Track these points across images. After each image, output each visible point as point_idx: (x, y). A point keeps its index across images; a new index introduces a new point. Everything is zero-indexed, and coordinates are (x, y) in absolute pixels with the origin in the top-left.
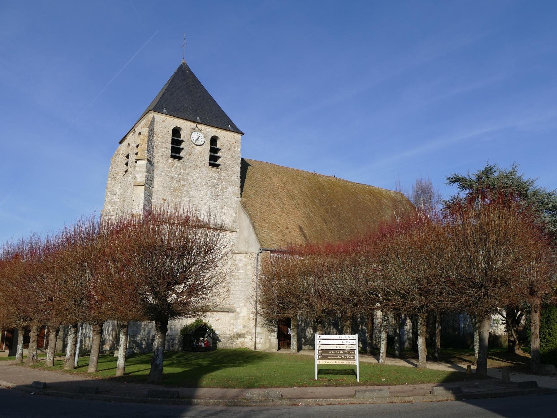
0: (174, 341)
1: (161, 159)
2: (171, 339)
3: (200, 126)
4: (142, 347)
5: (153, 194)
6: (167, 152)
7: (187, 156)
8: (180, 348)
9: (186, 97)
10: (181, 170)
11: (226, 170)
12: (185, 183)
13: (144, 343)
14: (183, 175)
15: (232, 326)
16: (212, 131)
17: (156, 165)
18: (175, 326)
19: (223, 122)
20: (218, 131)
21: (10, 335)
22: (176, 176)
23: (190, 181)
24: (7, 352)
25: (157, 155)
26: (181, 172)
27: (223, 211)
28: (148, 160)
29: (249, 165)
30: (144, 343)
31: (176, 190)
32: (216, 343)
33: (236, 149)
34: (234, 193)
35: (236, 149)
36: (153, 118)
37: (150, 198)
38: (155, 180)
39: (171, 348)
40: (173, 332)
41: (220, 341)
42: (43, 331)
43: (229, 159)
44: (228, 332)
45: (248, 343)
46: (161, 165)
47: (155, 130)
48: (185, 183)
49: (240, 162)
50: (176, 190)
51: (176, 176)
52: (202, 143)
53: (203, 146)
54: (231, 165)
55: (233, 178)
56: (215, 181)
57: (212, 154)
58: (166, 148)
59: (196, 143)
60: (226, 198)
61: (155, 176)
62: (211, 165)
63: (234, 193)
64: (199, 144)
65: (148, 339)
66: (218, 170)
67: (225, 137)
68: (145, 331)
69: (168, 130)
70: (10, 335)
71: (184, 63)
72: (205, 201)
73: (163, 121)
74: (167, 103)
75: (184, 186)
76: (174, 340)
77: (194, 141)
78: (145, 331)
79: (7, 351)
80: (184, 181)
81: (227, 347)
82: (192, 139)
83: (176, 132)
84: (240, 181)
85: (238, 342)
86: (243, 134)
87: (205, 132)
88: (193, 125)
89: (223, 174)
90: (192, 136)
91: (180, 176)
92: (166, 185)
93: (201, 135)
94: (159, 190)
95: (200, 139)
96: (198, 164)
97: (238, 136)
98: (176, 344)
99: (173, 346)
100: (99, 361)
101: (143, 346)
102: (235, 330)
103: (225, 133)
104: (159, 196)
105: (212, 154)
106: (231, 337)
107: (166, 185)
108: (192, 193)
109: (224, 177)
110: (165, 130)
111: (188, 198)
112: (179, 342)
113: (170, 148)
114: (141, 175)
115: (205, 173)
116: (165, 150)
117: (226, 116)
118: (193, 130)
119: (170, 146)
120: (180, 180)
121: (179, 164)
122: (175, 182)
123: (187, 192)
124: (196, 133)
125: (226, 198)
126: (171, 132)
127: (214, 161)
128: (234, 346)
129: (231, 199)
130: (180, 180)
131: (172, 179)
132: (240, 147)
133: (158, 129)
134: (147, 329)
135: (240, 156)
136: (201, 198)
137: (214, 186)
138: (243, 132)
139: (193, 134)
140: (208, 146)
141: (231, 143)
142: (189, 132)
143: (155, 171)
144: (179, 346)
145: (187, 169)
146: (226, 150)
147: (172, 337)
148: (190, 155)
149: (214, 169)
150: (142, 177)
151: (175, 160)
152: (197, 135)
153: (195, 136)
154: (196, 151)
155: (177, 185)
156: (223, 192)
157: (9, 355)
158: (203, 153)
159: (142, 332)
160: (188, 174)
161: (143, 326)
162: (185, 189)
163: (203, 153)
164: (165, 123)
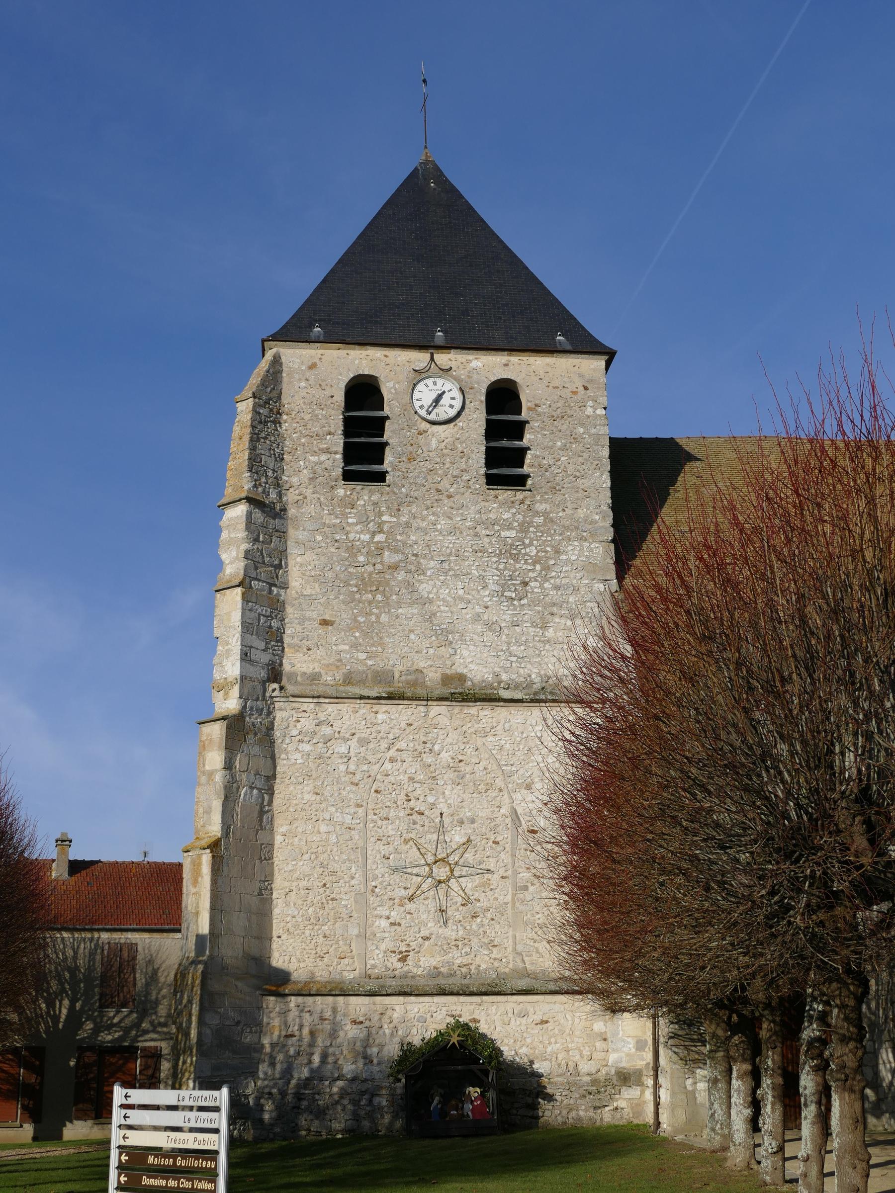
0: (376, 1100)
1: (308, 492)
2: (363, 1093)
3: (442, 358)
4: (261, 1120)
5: (289, 610)
6: (328, 464)
7: (403, 466)
8: (398, 1124)
9: (431, 270)
10: (380, 514)
11: (554, 490)
12: (400, 557)
13: (269, 1106)
14: (390, 532)
15: (599, 1044)
16: (488, 367)
17: (292, 512)
18: (381, 1046)
19: (547, 326)
20: (515, 359)
21: (33, 1079)
22: (366, 537)
23: (417, 549)
24: (28, 1129)
25: (295, 480)
26: (380, 525)
27: (550, 633)
28: (249, 500)
29: (691, 458)
30: (269, 1106)
31: (364, 584)
32: (535, 1107)
33: (589, 411)
34: (589, 568)
35: (589, 411)
36: (277, 361)
37: (275, 624)
38: (291, 563)
39: (366, 1124)
40: (376, 1069)
41: (550, 1098)
42: (131, 1065)
43: (564, 448)
44: (585, 1067)
45: (630, 1106)
46: (310, 509)
47: (285, 400)
48: (400, 557)
49: (606, 452)
50: (364, 584)
51: (366, 537)
52: (452, 413)
53: (460, 423)
54: (570, 469)
55: (581, 513)
56: (513, 534)
57: (493, 444)
58: (327, 451)
59: (432, 417)
60: (557, 588)
61: (293, 550)
62: (492, 481)
63: (589, 568)
64: (443, 417)
65: (283, 1093)
66: (520, 495)
67: (539, 376)
68: (273, 1064)
69: (328, 393)
70: (33, 1079)
71: (426, 162)
72: (478, 609)
73: (313, 366)
74: (351, 303)
75: (395, 567)
76: (373, 1095)
77: (423, 413)
78: (273, 1064)
79: (26, 1126)
80: (396, 551)
81: (580, 1119)
82: (417, 404)
83: (363, 393)
84: (610, 520)
85: (622, 1104)
86: (610, 355)
87: (463, 374)
88: (420, 358)
89: (540, 507)
90: (416, 395)
91: (378, 538)
92: (330, 575)
93: (448, 385)
94: (308, 592)
95: (446, 400)
96: (445, 484)
97: (599, 363)
98: (381, 1108)
99: (370, 1116)
100: (105, 1169)
101: (266, 1116)
102: (613, 1057)
103: (539, 362)
104: (308, 614)
105: (493, 444)
106: (595, 1082)
107: (330, 575)
108: (425, 588)
109: (545, 514)
110: (319, 394)
111: (411, 605)
112: (392, 1103)
113: (340, 449)
114: (234, 554)
115: (472, 512)
116: (324, 457)
117: (555, 303)
118: (420, 375)
119: (338, 442)
120: (380, 549)
121: (374, 498)
122: (361, 559)
123: (409, 585)
124: (429, 381)
125: (557, 588)
126: (340, 397)
127: (505, 462)
128: (606, 1116)
129: (576, 590)
130: (380, 549)
131: (352, 549)
132: (604, 400)
133: (295, 394)
134: (280, 1057)
135: (604, 432)
136: (461, 599)
137: (510, 552)
138: (608, 342)
139: (421, 386)
140: (477, 419)
141: (566, 393)
142: (405, 385)
143: (292, 533)
144: (395, 1117)
145: (405, 510)
146: (548, 422)
147: (369, 1085)
148: (411, 459)
149: (506, 494)
150: (237, 558)
151: (358, 486)
152: (434, 394)
153: (425, 394)
154: (434, 443)
155: (370, 568)
156: (547, 568)
157: (35, 1139)
158: (460, 447)
159: (263, 1068)
160: (408, 525)
161: (268, 1049)
162: (401, 576)
163: (460, 447)
164: (317, 374)
